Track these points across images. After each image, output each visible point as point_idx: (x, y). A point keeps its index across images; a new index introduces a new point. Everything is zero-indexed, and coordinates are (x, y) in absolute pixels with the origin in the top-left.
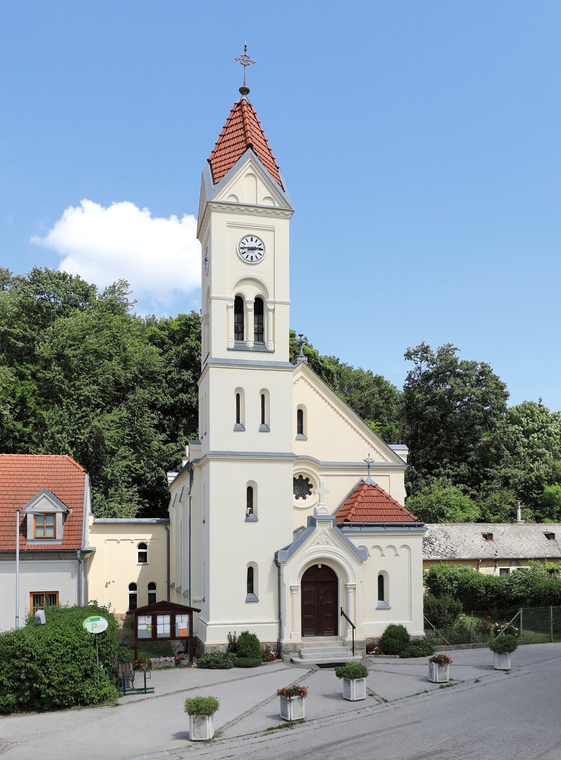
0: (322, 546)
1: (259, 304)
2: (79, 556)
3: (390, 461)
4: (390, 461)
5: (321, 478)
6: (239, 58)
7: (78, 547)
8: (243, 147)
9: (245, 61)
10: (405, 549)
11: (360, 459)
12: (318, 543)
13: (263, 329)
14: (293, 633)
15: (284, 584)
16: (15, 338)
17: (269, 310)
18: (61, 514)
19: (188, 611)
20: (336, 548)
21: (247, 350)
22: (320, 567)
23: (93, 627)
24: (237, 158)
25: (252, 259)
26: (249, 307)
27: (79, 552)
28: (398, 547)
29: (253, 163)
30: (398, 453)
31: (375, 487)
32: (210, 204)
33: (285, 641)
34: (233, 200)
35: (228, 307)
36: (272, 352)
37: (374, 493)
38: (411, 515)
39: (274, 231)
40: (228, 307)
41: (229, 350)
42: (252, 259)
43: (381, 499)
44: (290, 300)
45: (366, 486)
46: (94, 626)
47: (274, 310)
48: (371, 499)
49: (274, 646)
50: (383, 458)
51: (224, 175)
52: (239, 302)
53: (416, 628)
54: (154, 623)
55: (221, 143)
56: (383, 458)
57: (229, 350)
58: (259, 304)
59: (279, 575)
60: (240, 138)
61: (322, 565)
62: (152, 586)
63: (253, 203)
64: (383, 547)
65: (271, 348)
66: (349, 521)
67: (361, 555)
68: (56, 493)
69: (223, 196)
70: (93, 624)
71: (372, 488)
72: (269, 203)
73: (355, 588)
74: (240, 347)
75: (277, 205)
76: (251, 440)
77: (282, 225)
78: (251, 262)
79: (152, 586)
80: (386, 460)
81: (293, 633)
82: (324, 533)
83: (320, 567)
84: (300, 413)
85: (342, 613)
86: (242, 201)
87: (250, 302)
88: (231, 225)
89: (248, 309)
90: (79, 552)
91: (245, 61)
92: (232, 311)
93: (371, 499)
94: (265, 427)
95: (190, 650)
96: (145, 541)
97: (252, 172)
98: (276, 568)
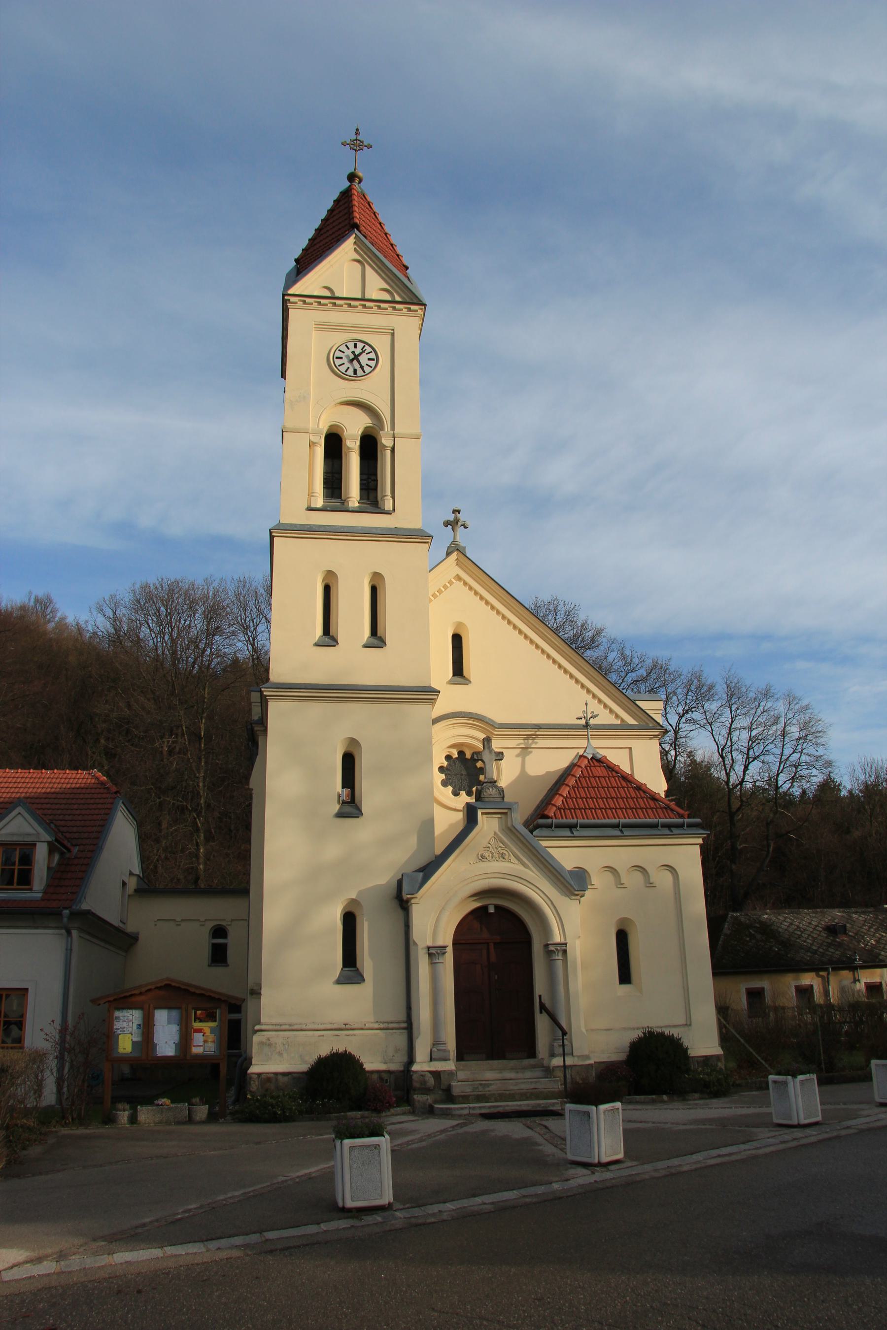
1: (370, 446)
2: (65, 920)
3: (631, 721)
16: (200, 762)
21: (344, 509)
22: (492, 910)
27: (66, 912)
30: (643, 705)
33: (422, 1065)
35: (312, 445)
44: (720, 1049)
47: (393, 450)
50: (617, 716)
52: (334, 443)
53: (703, 1041)
54: (147, 1027)
56: (617, 716)
58: (370, 446)
60: (341, 221)
61: (497, 907)
66: (547, 817)
68: (62, 829)
73: (565, 952)
77: (405, 324)
81: (435, 1049)
83: (492, 910)
84: (457, 641)
85: (543, 1007)
87: (352, 438)
88: (322, 327)
89: (349, 448)
90: (66, 912)
94: (377, 638)
95: (219, 1084)
96: (224, 923)
97: (359, 258)
98: (401, 913)
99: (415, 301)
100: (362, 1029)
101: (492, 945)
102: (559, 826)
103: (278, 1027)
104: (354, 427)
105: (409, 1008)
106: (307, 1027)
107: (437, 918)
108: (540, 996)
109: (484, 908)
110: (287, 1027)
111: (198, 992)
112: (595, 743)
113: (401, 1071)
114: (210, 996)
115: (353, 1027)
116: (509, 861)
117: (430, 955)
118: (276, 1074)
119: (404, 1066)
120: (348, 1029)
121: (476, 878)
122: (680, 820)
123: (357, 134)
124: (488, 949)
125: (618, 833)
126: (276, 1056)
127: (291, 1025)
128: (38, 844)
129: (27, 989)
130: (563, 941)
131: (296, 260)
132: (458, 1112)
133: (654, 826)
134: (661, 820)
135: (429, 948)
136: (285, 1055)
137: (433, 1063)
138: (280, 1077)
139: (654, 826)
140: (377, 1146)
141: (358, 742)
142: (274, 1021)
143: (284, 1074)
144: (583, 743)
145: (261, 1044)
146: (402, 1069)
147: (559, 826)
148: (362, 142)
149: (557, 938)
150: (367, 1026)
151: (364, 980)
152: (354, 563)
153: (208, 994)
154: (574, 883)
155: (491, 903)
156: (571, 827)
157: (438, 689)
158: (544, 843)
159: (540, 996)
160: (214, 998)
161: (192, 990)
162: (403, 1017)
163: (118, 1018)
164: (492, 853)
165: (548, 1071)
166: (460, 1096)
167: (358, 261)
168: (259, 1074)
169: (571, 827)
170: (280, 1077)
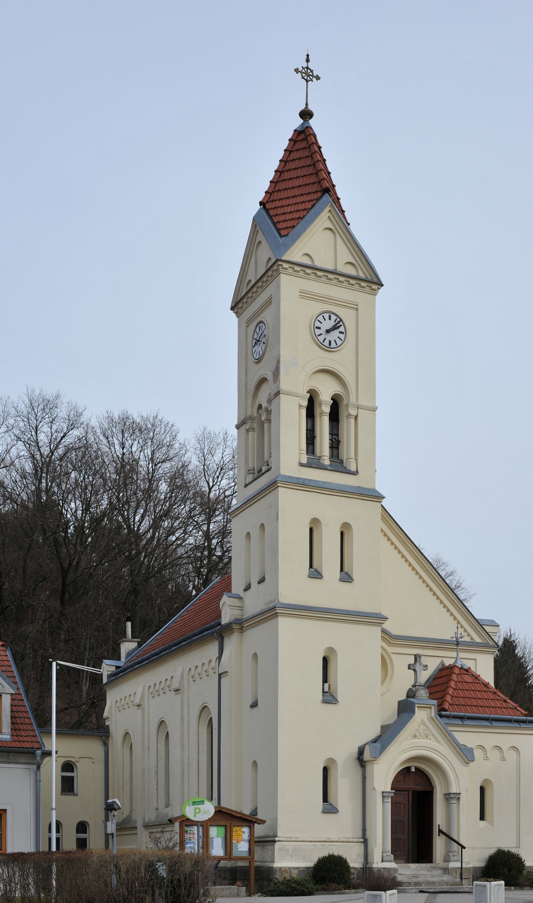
0: (422, 739)
4: (478, 639)
5: (393, 656)
6: (300, 70)
7: (36, 745)
8: (317, 192)
9: (308, 75)
10: (513, 752)
11: (448, 634)
12: (415, 736)
13: (338, 442)
14: (381, 859)
15: (374, 789)
17: (349, 415)
18: (9, 697)
19: (249, 821)
20: (437, 744)
21: (323, 468)
22: (413, 770)
23: (195, 813)
24: (309, 205)
25: (330, 344)
26: (324, 409)
27: (39, 752)
28: (505, 749)
29: (332, 214)
31: (468, 670)
32: (280, 263)
34: (306, 261)
35: (300, 406)
36: (356, 473)
37: (467, 678)
38: (518, 708)
39: (357, 310)
40: (300, 406)
41: (301, 465)
42: (330, 344)
43: (478, 687)
45: (458, 669)
46: (197, 811)
47: (356, 417)
48: (466, 686)
49: (358, 872)
51: (294, 227)
55: (278, 182)
57: (301, 465)
59: (364, 778)
62: (82, 827)
63: (331, 267)
64: (488, 748)
65: (353, 468)
67: (466, 755)
69: (295, 253)
70: (195, 809)
71: (465, 672)
72: (351, 271)
73: (459, 798)
74: (313, 463)
75: (362, 275)
76: (328, 592)
78: (329, 348)
79: (82, 827)
80: (472, 638)
81: (384, 855)
82: (423, 722)
83: (413, 770)
86: (318, 264)
88: (305, 295)
90: (39, 752)
91: (308, 75)
92: (304, 412)
93: (466, 686)
97: (331, 226)
98: (360, 769)
99: (375, 280)
100: (338, 842)
101: (411, 792)
102: (455, 717)
103: (289, 839)
104: (327, 391)
105: (364, 830)
106: (306, 840)
107: (384, 773)
108: (439, 825)
109: (408, 768)
110: (294, 839)
111: (238, 815)
112: (462, 655)
113: (361, 868)
114: (245, 819)
115: (333, 840)
116: (430, 739)
117: (383, 796)
118: (290, 868)
119: (363, 865)
120: (329, 842)
121: (409, 750)
122: (525, 718)
123: (308, 61)
124: (409, 794)
125: (489, 724)
126: (291, 858)
127: (296, 838)
128: (3, 695)
129: (5, 810)
130: (458, 792)
131: (261, 203)
132: (409, 891)
133: (509, 721)
134: (514, 717)
135: (383, 792)
136: (294, 856)
137: (383, 863)
138: (292, 870)
139: (509, 721)
140: (485, 886)
141: (335, 650)
142: (285, 836)
143: (294, 868)
144: (454, 654)
145: (280, 849)
146: (362, 866)
147: (455, 717)
148: (312, 71)
149: (454, 790)
150: (341, 840)
151: (338, 811)
152: (333, 512)
153: (244, 817)
154: (466, 755)
155: (413, 765)
156: (461, 718)
157: (387, 617)
158: (450, 728)
159: (439, 825)
160: (248, 820)
161: (235, 814)
162: (360, 834)
163: (187, 831)
164: (420, 733)
165: (446, 870)
166: (406, 883)
167: (330, 229)
168: (280, 868)
169: (461, 718)
170: (292, 870)
